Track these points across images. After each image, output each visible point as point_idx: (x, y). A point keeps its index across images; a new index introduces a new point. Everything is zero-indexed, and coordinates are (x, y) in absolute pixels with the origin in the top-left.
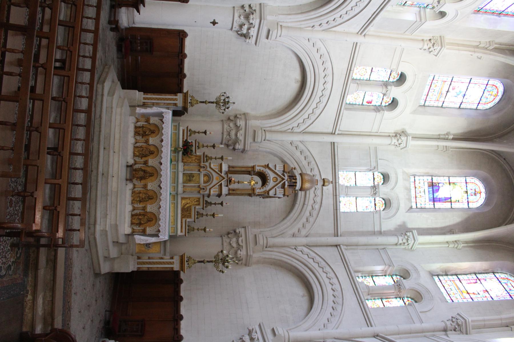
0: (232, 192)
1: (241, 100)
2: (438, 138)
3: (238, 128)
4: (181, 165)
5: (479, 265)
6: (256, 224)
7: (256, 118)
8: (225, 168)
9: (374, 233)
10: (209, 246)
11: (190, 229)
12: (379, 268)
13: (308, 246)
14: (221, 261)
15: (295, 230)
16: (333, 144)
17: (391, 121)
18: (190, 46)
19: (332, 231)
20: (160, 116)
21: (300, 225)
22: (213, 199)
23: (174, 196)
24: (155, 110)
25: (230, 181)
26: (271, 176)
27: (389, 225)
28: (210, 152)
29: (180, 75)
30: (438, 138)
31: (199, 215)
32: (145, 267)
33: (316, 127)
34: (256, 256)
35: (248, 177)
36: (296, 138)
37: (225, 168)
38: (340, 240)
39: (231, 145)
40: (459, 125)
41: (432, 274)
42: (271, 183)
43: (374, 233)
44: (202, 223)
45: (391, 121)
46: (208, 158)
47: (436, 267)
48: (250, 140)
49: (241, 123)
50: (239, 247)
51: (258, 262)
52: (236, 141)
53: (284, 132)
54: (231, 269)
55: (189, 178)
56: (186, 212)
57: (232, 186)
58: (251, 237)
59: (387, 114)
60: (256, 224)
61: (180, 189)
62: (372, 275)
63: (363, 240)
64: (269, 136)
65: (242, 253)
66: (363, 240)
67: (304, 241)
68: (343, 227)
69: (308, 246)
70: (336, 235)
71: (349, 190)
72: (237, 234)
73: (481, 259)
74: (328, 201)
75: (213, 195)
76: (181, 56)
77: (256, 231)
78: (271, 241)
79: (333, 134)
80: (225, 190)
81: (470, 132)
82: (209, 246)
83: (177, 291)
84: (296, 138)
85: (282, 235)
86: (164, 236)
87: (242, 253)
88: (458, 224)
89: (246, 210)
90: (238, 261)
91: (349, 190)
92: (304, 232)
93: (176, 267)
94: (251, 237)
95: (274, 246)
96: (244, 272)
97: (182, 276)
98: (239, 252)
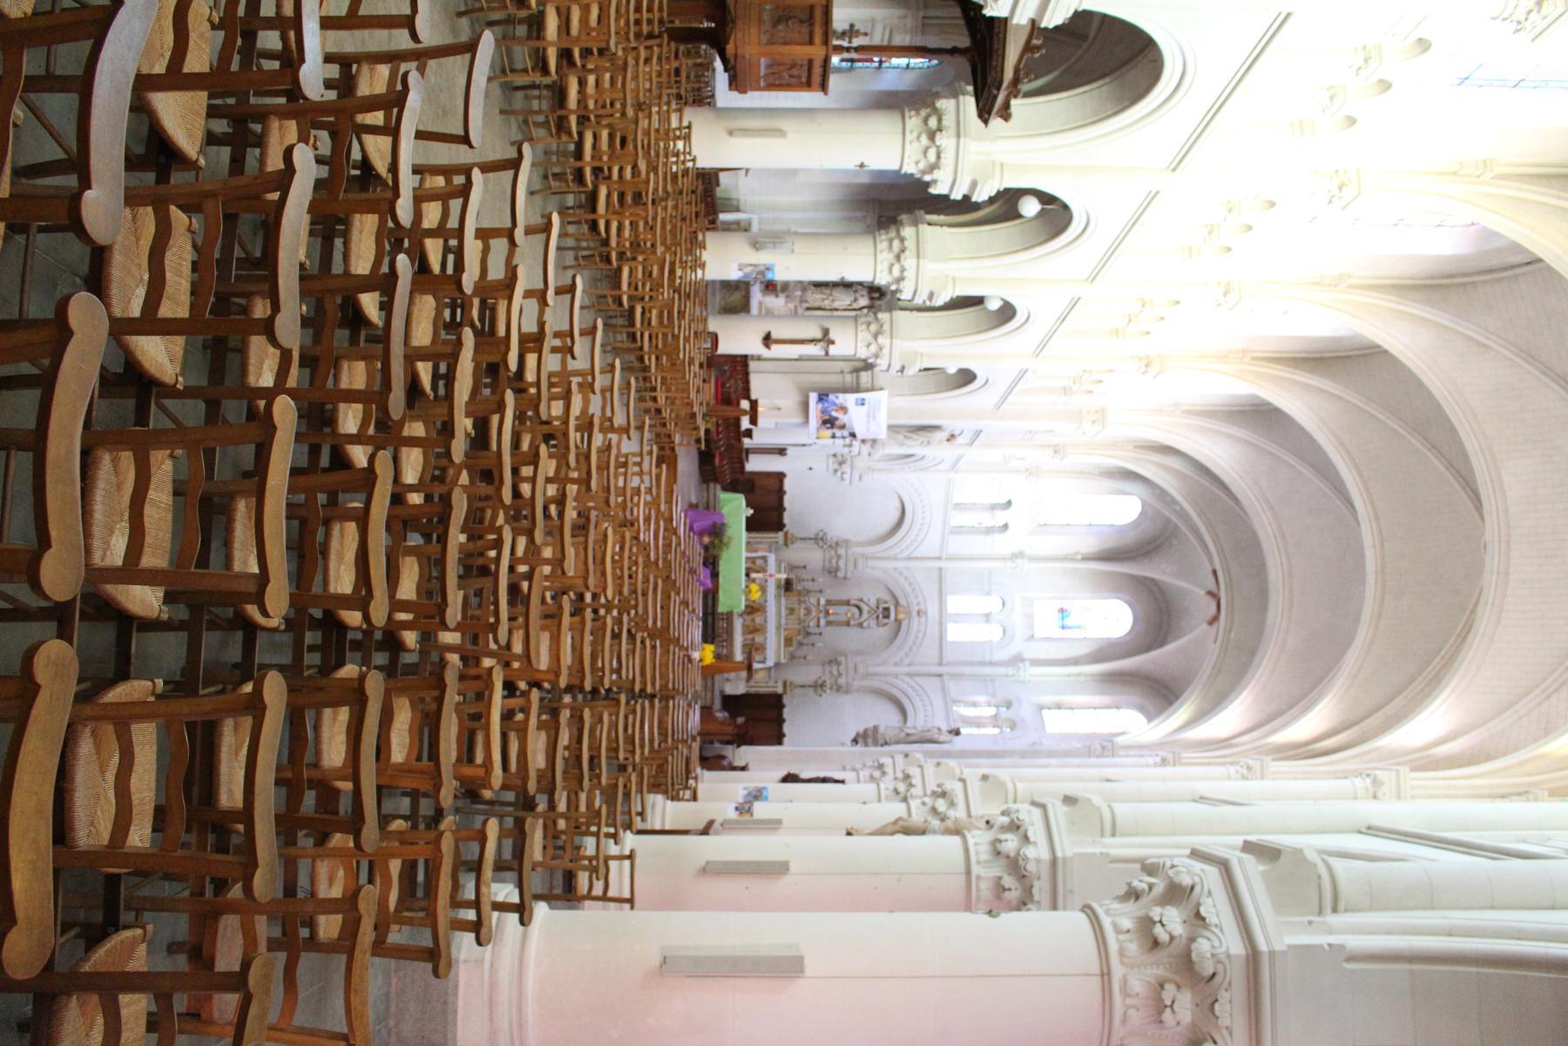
0: (829, 623)
1: (839, 526)
2: (1065, 559)
3: (839, 557)
4: (783, 601)
5: (1105, 699)
6: (860, 653)
7: (859, 544)
8: (822, 602)
9: (984, 664)
10: (810, 674)
11: (792, 657)
12: (982, 699)
13: (910, 675)
14: (819, 686)
15: (897, 659)
16: (940, 569)
17: (1003, 544)
18: (788, 484)
19: (937, 660)
20: (765, 558)
21: (902, 654)
22: (813, 630)
23: (778, 628)
24: (760, 554)
25: (827, 613)
26: (865, 609)
27: (1004, 655)
28: (809, 585)
29: (780, 508)
30: (1072, 559)
31: (801, 644)
32: (753, 690)
33: (921, 552)
34: (856, 684)
35: (845, 608)
36: (900, 565)
37: (822, 602)
38: (947, 670)
39: (832, 572)
40: (1090, 544)
41: (1041, 707)
42: (865, 615)
43: (984, 664)
44: (804, 650)
45: (1003, 544)
46: (809, 592)
47: (1047, 699)
48: (851, 568)
49: (841, 551)
50: (840, 675)
51: (858, 690)
52: (837, 569)
53: (887, 559)
54: (828, 697)
55: (791, 611)
56: (788, 641)
57: (831, 618)
58: (851, 665)
59: (997, 537)
60: (860, 653)
61: (783, 621)
62: (974, 704)
63: (968, 670)
64: (870, 563)
65: (842, 681)
66: (968, 670)
67: (905, 669)
68: (949, 656)
69: (910, 675)
70: (940, 664)
71: (958, 618)
72: (838, 663)
73: (1107, 693)
74: (933, 630)
75: (235, 882)
76: (781, 492)
77: (857, 659)
78: (873, 669)
79: (939, 558)
80: (822, 622)
81: (1108, 550)
82: (810, 674)
83: (780, 714)
84: (900, 565)
85: (884, 663)
86: (770, 663)
87: (842, 681)
88: (1087, 655)
89: (848, 639)
90: (839, 689)
91: (958, 618)
92: (906, 661)
93: (780, 690)
94: (851, 665)
95: (874, 675)
96: (845, 699)
97: (786, 700)
98: (1203, 946)
